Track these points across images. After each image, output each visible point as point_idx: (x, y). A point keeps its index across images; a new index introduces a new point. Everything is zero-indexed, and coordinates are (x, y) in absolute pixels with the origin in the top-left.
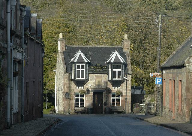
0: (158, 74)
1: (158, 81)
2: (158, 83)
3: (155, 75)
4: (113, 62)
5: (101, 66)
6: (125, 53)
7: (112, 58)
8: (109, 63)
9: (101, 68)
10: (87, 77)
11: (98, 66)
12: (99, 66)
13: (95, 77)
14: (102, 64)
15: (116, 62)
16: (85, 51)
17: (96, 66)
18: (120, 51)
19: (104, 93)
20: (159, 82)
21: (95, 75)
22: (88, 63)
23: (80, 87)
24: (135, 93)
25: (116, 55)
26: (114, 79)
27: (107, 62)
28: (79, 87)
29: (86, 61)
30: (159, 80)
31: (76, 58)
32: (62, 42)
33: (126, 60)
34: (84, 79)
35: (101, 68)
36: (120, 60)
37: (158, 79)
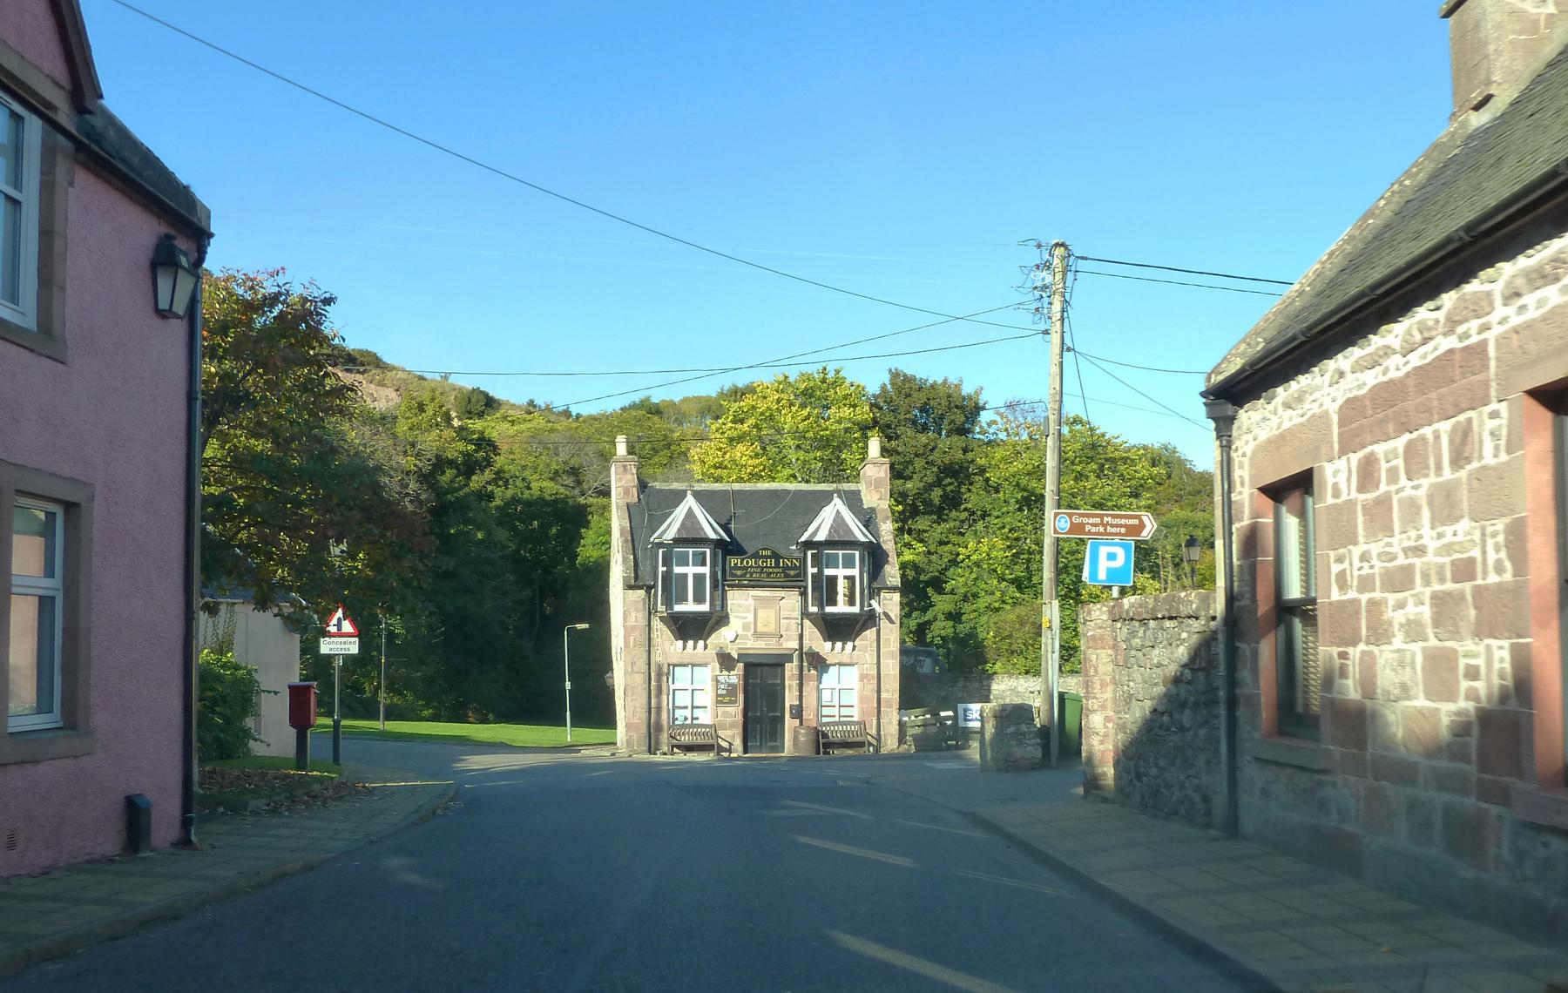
0: (1101, 517)
1: (1104, 566)
2: (1102, 575)
3: (1083, 525)
4: (821, 536)
5: (776, 556)
6: (873, 510)
7: (821, 527)
8: (809, 544)
9: (777, 563)
10: (718, 603)
11: (762, 557)
12: (767, 557)
13: (751, 602)
14: (782, 552)
15: (837, 539)
16: (699, 496)
17: (756, 556)
18: (853, 500)
19: (791, 669)
20: (1109, 570)
21: (753, 592)
22: (719, 544)
23: (690, 643)
24: (831, 643)
25: (838, 512)
26: (829, 609)
27: (803, 539)
28: (685, 641)
29: (713, 536)
30: (1111, 557)
31: (670, 529)
32: (624, 467)
33: (876, 534)
34: (705, 608)
35: (777, 563)
36: (852, 532)
37: (1104, 551)
